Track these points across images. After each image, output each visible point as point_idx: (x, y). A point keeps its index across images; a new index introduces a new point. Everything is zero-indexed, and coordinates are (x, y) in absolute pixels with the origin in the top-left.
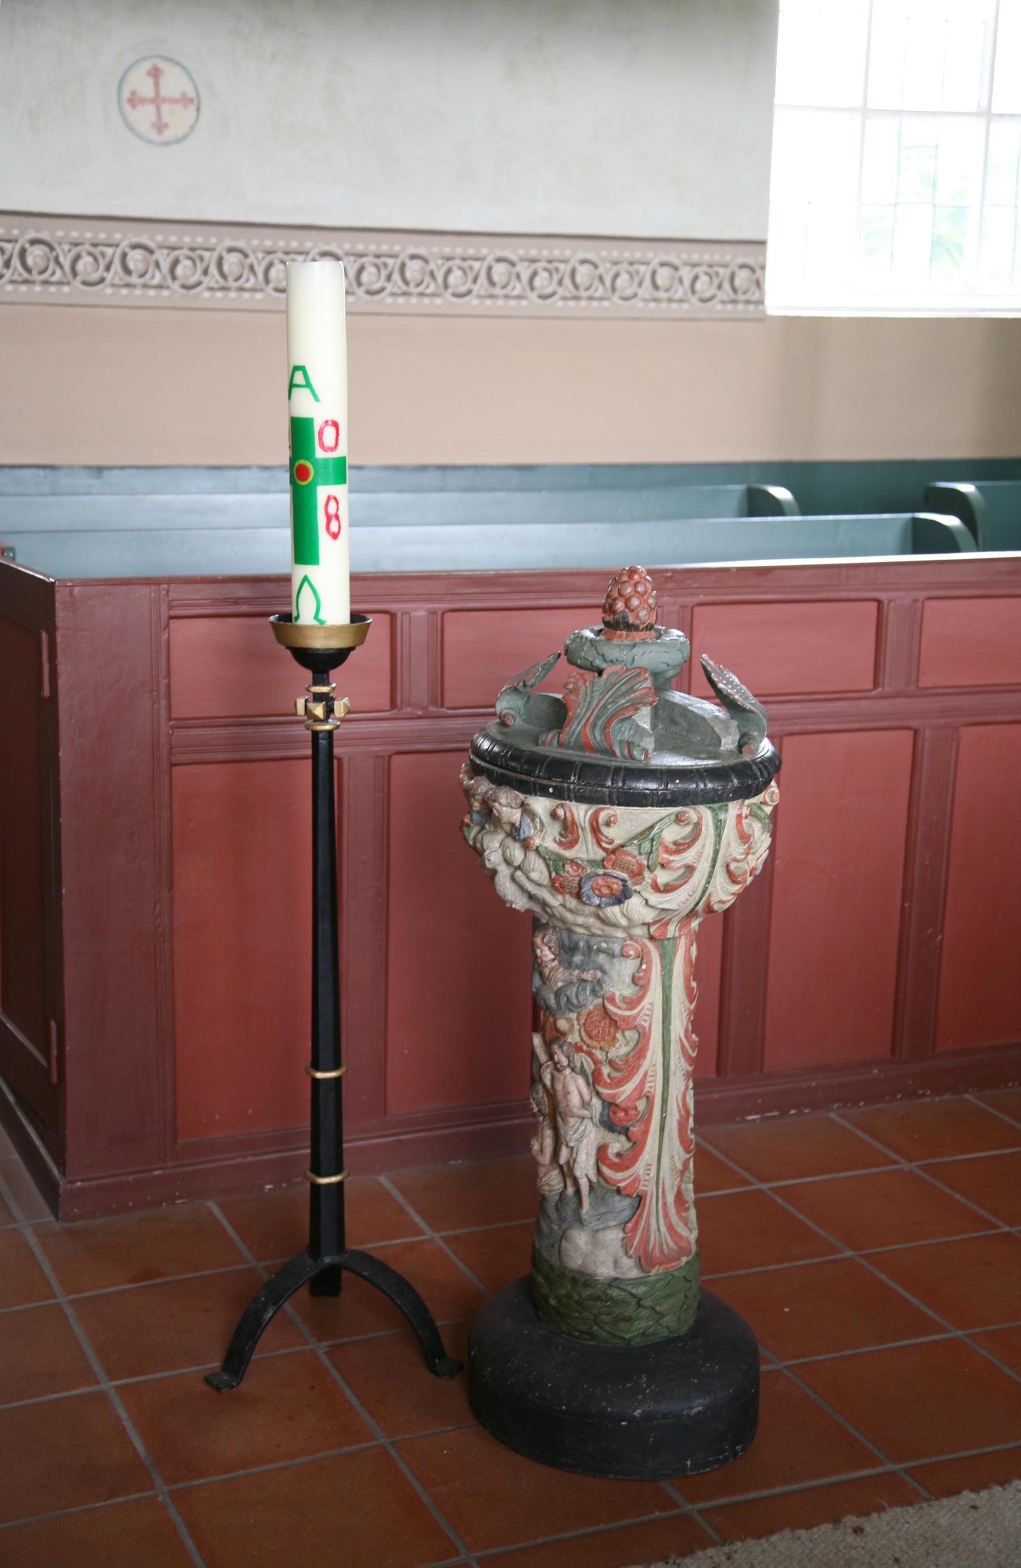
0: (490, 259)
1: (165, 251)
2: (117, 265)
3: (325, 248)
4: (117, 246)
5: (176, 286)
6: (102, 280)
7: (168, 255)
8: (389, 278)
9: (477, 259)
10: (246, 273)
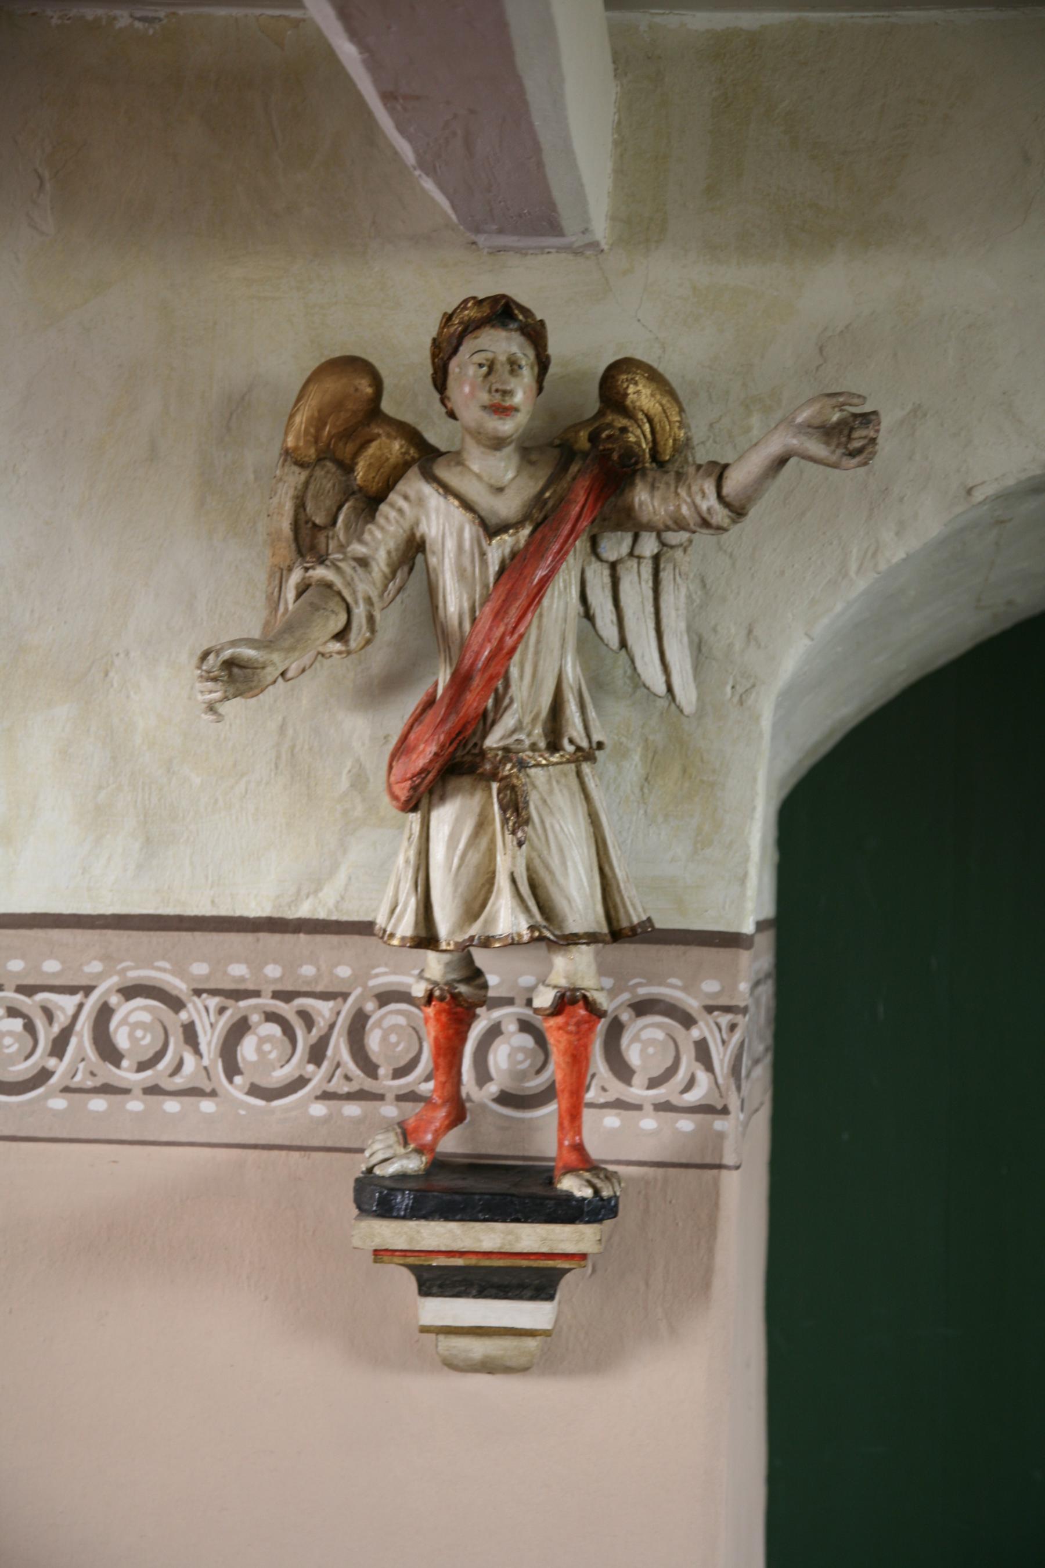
0: (105, 989)
1: (213, 1002)
2: (82, 1038)
3: (137, 975)
4: (88, 990)
5: (236, 1090)
6: (43, 1076)
7: (222, 1010)
8: (317, 1054)
9: (72, 990)
10: (688, 1063)
